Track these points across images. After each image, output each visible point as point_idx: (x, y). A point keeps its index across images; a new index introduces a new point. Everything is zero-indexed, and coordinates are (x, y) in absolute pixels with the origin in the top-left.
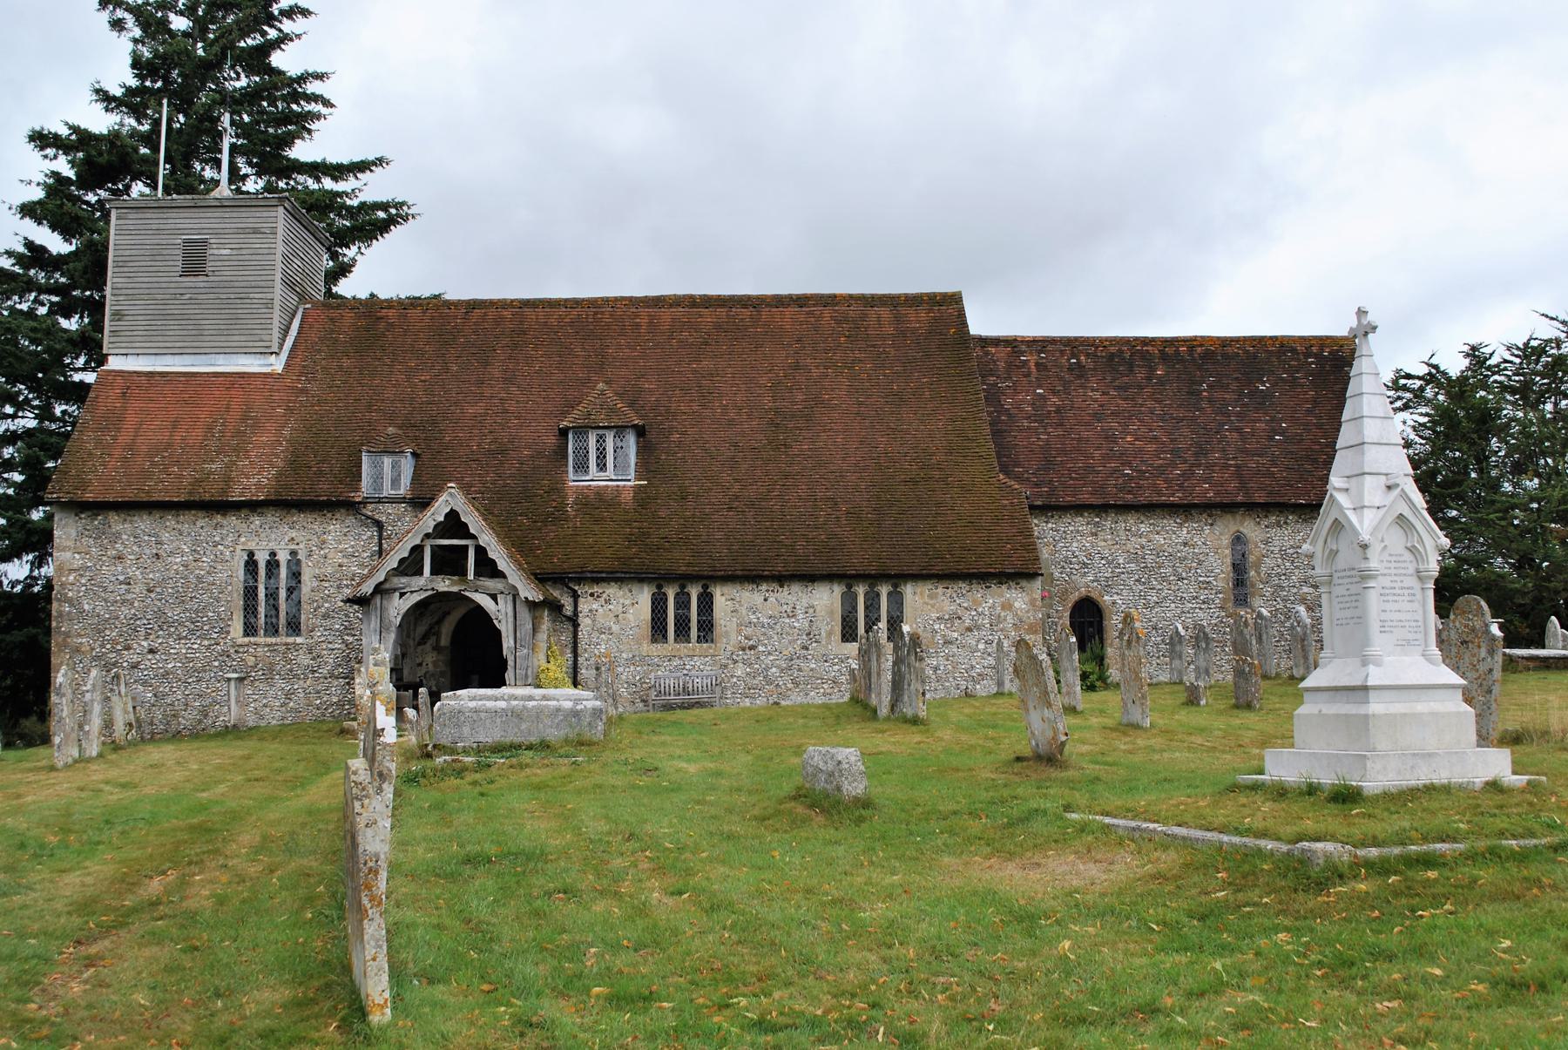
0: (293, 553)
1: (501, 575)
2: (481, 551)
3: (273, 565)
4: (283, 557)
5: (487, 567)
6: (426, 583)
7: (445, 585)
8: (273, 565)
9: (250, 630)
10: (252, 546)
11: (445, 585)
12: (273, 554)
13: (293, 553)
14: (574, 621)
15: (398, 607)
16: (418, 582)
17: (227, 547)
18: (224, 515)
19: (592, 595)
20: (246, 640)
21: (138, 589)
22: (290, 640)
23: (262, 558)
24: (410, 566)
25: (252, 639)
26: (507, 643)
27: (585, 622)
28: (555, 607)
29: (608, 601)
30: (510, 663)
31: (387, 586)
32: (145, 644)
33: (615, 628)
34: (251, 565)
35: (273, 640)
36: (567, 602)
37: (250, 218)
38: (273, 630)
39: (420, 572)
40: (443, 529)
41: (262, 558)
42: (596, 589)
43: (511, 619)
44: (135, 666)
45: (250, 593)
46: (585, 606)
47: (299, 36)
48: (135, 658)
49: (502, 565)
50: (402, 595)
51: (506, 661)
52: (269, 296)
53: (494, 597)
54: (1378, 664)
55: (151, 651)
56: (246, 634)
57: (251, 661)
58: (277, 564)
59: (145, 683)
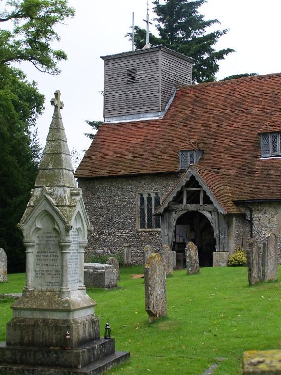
0: (157, 194)
1: (211, 203)
2: (204, 192)
3: (149, 199)
4: (153, 196)
5: (207, 201)
6: (186, 206)
7: (192, 207)
8: (149, 199)
9: (143, 226)
10: (141, 192)
11: (192, 207)
12: (149, 195)
13: (157, 194)
14: (251, 222)
15: (174, 217)
16: (181, 206)
17: (133, 193)
18: (132, 180)
19: (258, 210)
20: (141, 230)
21: (105, 210)
22: (156, 230)
23: (145, 196)
24: (178, 199)
25: (143, 230)
26: (216, 233)
27: (256, 222)
28: (242, 217)
29: (265, 213)
30: (217, 241)
31: (170, 209)
32: (107, 231)
33: (268, 225)
34: (142, 199)
35: (150, 230)
36: (248, 213)
37: (151, 57)
38: (150, 226)
39: (182, 202)
40: (188, 184)
41: (145, 196)
42: (260, 208)
43: (217, 222)
44: (104, 240)
45: (142, 210)
46: (256, 215)
47: (225, 32)
48: (105, 238)
49: (212, 198)
50: (176, 212)
51: (216, 241)
52: (157, 88)
53: (210, 212)
54: (37, 89)
55: (110, 235)
56: (141, 228)
57: (143, 238)
58: (151, 198)
59: (108, 247)
